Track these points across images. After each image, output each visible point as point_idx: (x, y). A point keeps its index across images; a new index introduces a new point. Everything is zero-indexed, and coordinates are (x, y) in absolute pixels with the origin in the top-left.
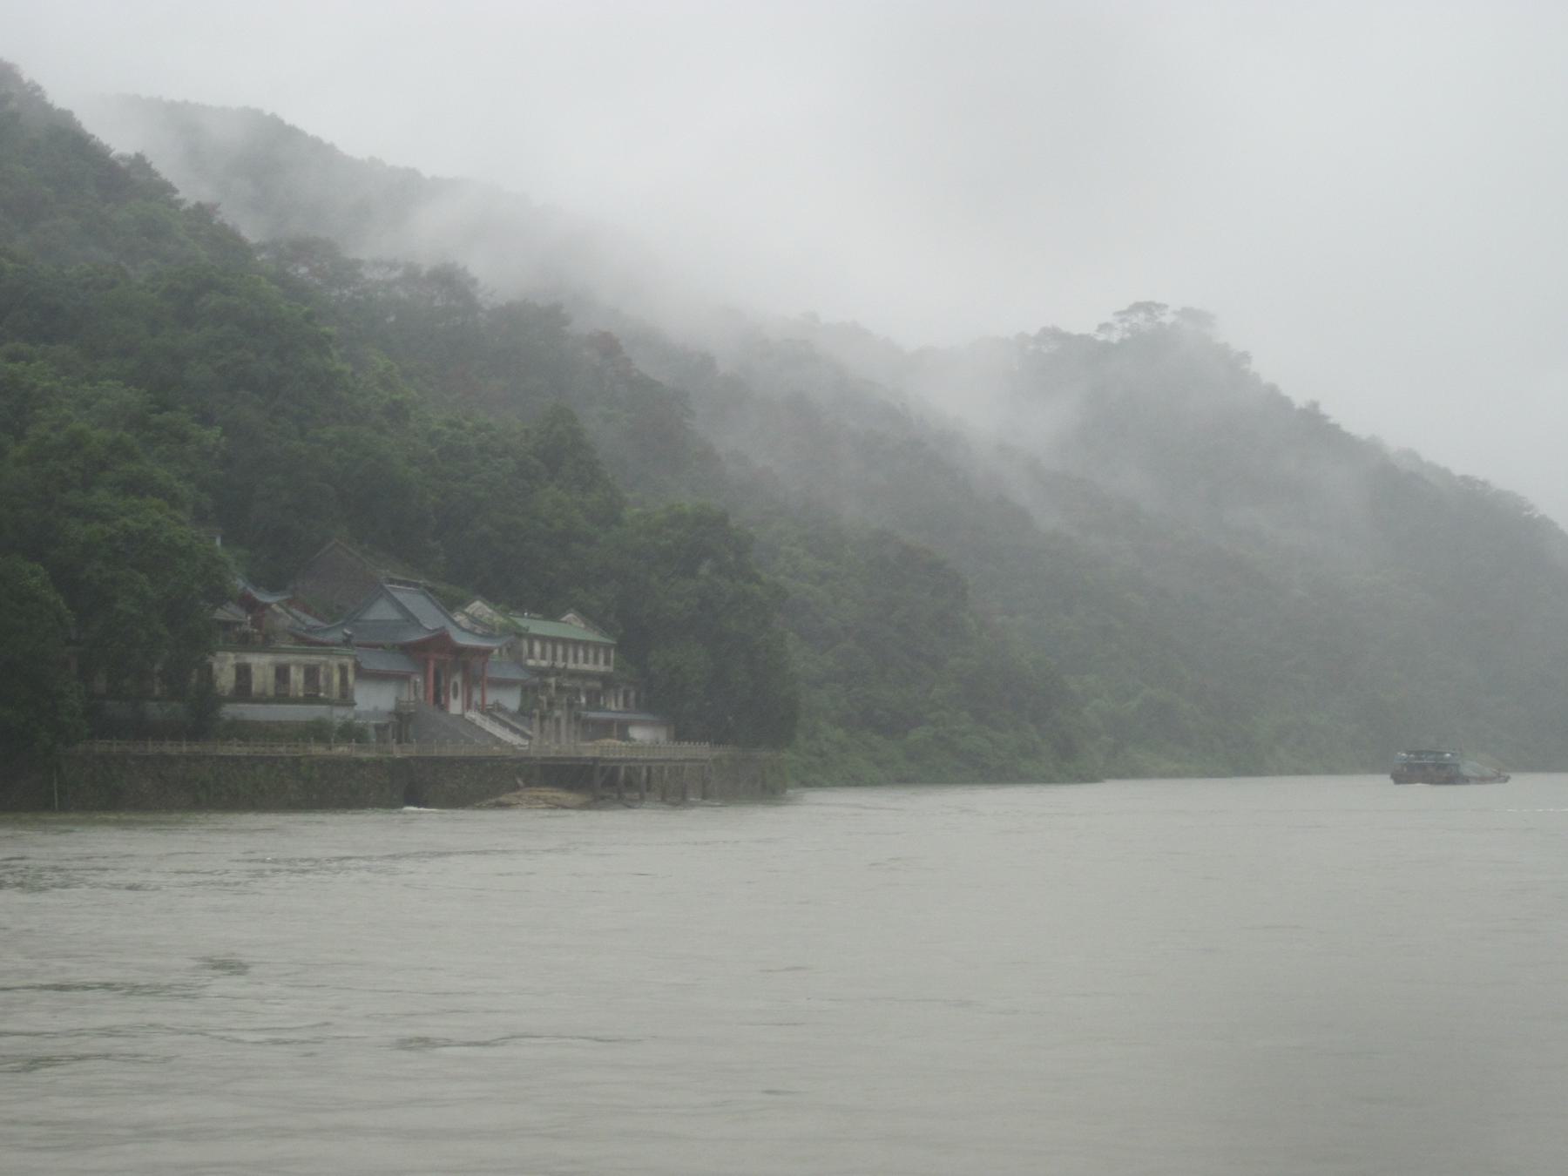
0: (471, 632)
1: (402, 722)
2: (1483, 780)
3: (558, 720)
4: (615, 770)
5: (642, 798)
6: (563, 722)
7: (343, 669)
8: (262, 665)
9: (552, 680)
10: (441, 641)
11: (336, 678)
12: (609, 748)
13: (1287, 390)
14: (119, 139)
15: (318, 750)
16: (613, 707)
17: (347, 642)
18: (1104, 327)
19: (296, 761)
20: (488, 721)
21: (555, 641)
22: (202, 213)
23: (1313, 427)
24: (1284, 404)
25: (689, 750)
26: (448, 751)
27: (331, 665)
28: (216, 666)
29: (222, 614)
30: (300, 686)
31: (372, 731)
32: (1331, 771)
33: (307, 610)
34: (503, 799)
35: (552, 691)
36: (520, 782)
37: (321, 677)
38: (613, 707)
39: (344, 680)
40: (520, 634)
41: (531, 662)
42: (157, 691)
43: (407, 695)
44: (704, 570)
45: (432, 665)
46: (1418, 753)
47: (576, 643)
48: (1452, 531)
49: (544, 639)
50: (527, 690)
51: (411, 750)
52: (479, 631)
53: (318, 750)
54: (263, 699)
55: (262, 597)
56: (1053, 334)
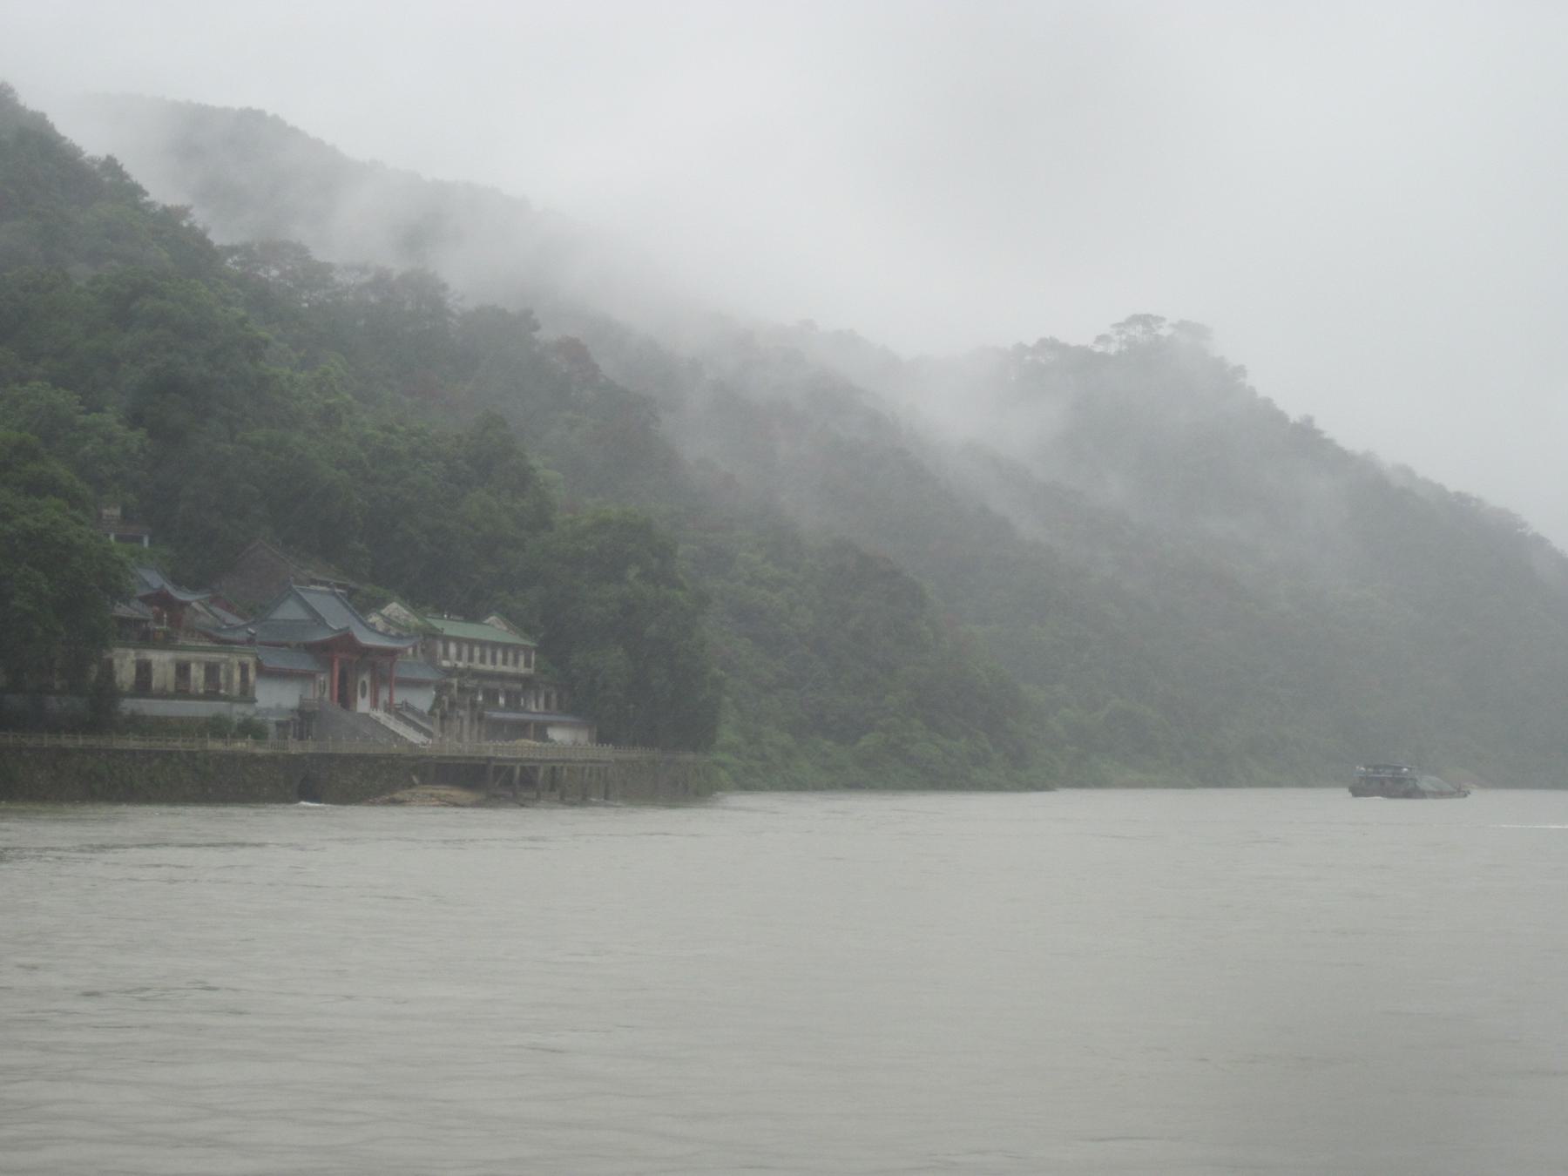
0: (384, 634)
1: (303, 721)
2: (1440, 794)
3: (461, 719)
4: (511, 771)
5: (538, 797)
6: (466, 723)
7: (244, 668)
8: (162, 661)
9: (455, 681)
10: (346, 642)
11: (237, 676)
12: (526, 747)
13: (1281, 404)
14: (90, 137)
15: (217, 746)
16: (534, 709)
17: (250, 641)
18: (1102, 339)
19: (192, 755)
20: (394, 719)
21: (472, 643)
22: (170, 217)
23: (1305, 441)
24: (1280, 418)
25: (607, 752)
26: (346, 747)
27: (232, 663)
28: (116, 662)
29: (122, 610)
30: (201, 681)
31: (272, 729)
32: (1303, 783)
33: (228, 607)
34: (397, 796)
35: (454, 691)
36: (415, 779)
37: (222, 675)
38: (534, 708)
39: (244, 679)
40: (431, 635)
41: (445, 663)
42: (57, 685)
43: (312, 693)
44: (632, 572)
45: (337, 667)
46: (1376, 767)
47: (495, 645)
48: (1442, 548)
49: (459, 641)
50: (442, 688)
51: (310, 747)
52: (393, 633)
53: (217, 746)
54: (163, 695)
55: (181, 596)
56: (1049, 345)
